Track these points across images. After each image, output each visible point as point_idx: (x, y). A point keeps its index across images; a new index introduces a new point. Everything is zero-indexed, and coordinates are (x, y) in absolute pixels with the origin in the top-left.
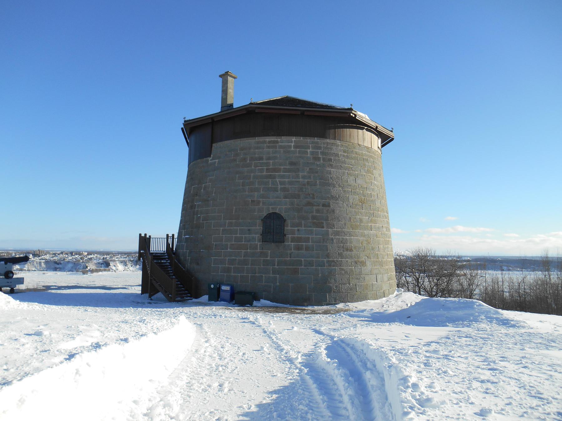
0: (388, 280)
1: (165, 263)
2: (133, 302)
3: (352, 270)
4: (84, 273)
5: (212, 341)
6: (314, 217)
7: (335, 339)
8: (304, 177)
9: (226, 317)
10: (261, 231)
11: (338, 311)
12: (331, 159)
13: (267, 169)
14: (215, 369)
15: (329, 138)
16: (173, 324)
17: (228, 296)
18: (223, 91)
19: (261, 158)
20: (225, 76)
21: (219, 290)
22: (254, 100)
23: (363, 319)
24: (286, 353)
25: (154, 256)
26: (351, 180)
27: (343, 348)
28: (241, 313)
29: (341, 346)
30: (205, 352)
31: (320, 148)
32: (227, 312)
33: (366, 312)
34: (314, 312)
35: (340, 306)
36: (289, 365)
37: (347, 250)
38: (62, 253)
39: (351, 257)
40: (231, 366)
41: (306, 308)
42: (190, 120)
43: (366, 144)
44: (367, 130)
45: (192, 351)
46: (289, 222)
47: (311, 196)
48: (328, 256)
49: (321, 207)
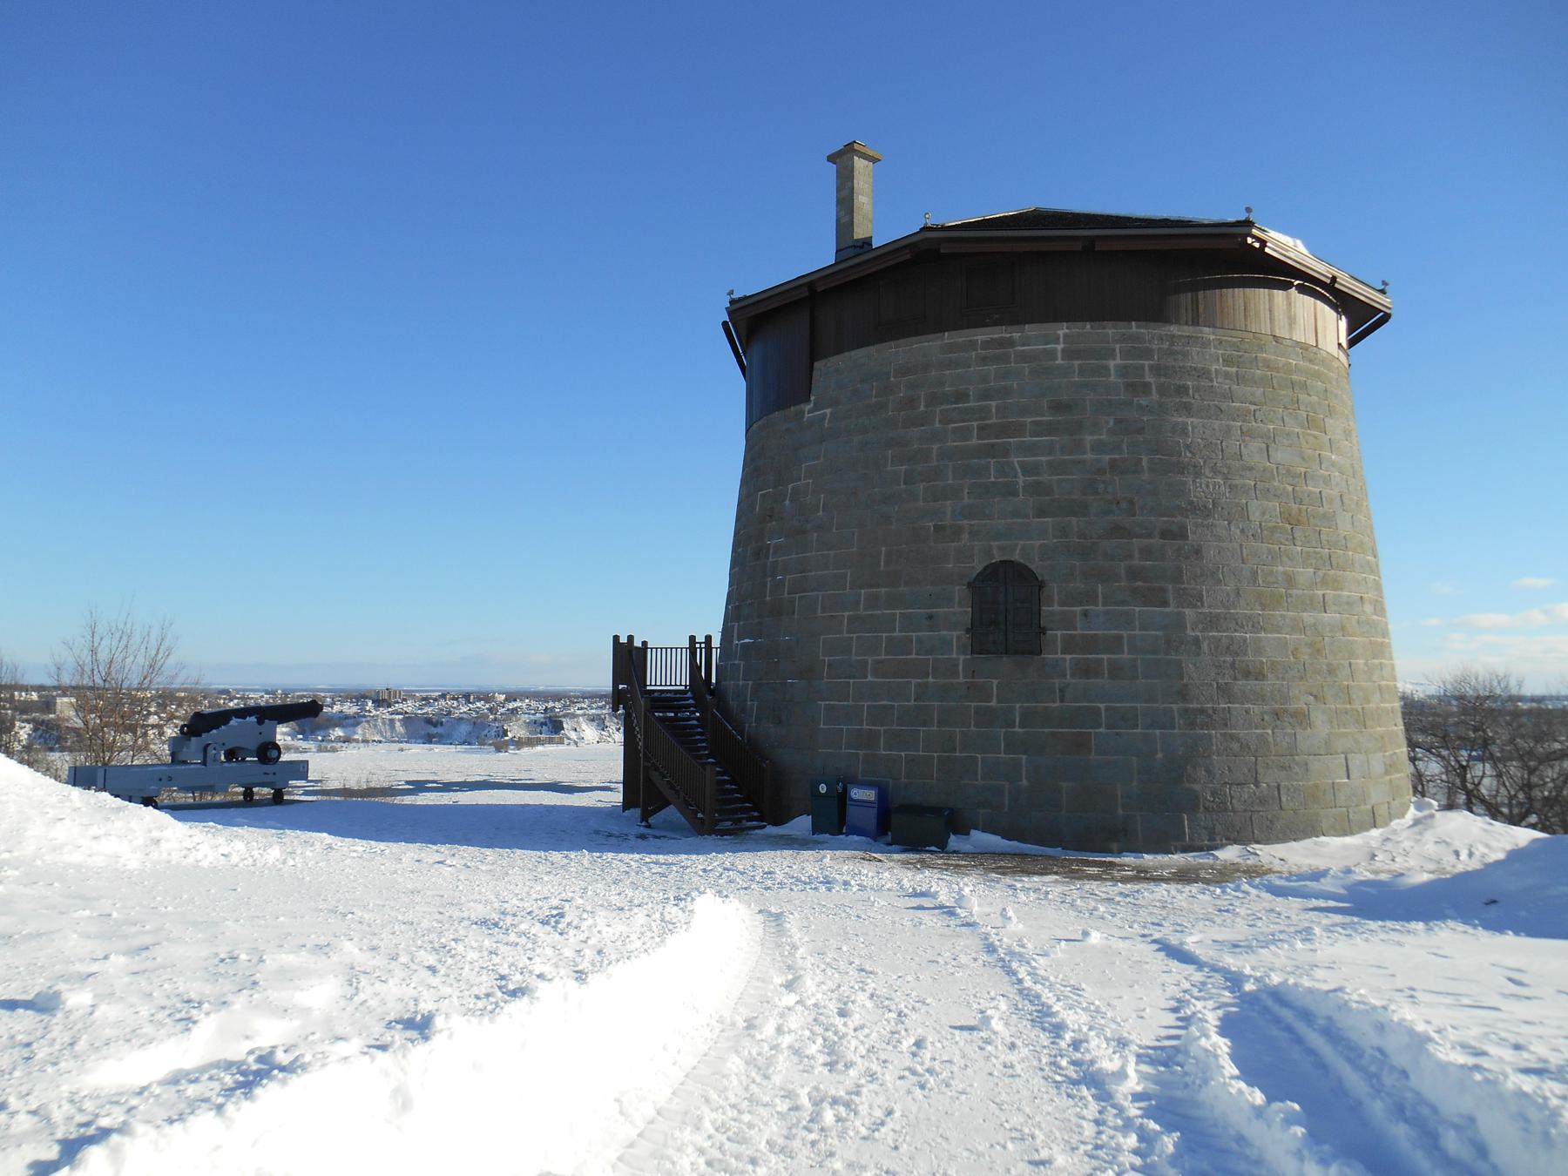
0: (1387, 772)
1: (689, 719)
2: (597, 832)
3: (1262, 739)
4: (498, 750)
5: (809, 984)
6: (1134, 574)
7: (1249, 987)
8: (1098, 448)
9: (862, 888)
10: (967, 619)
11: (1223, 876)
12: (1186, 388)
13: (981, 428)
14: (806, 1116)
15: (1177, 322)
16: (668, 927)
17: (870, 818)
18: (840, 202)
19: (961, 397)
20: (843, 158)
21: (843, 798)
22: (934, 220)
23: (1322, 903)
24: (1076, 1045)
25: (654, 700)
26: (1253, 451)
27: (1289, 1029)
28: (910, 874)
29: (1277, 1020)
30: (779, 1030)
31: (1147, 353)
32: (867, 870)
33: (1328, 879)
34: (1143, 876)
35: (1229, 854)
36: (1093, 1109)
37: (1247, 674)
38: (443, 696)
39: (1260, 698)
40: (869, 1104)
41: (1117, 860)
42: (746, 298)
43: (1299, 336)
44: (1302, 290)
45: (733, 1024)
46: (1054, 589)
47: (1124, 505)
48: (1183, 695)
49: (1156, 541)
